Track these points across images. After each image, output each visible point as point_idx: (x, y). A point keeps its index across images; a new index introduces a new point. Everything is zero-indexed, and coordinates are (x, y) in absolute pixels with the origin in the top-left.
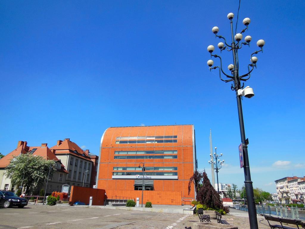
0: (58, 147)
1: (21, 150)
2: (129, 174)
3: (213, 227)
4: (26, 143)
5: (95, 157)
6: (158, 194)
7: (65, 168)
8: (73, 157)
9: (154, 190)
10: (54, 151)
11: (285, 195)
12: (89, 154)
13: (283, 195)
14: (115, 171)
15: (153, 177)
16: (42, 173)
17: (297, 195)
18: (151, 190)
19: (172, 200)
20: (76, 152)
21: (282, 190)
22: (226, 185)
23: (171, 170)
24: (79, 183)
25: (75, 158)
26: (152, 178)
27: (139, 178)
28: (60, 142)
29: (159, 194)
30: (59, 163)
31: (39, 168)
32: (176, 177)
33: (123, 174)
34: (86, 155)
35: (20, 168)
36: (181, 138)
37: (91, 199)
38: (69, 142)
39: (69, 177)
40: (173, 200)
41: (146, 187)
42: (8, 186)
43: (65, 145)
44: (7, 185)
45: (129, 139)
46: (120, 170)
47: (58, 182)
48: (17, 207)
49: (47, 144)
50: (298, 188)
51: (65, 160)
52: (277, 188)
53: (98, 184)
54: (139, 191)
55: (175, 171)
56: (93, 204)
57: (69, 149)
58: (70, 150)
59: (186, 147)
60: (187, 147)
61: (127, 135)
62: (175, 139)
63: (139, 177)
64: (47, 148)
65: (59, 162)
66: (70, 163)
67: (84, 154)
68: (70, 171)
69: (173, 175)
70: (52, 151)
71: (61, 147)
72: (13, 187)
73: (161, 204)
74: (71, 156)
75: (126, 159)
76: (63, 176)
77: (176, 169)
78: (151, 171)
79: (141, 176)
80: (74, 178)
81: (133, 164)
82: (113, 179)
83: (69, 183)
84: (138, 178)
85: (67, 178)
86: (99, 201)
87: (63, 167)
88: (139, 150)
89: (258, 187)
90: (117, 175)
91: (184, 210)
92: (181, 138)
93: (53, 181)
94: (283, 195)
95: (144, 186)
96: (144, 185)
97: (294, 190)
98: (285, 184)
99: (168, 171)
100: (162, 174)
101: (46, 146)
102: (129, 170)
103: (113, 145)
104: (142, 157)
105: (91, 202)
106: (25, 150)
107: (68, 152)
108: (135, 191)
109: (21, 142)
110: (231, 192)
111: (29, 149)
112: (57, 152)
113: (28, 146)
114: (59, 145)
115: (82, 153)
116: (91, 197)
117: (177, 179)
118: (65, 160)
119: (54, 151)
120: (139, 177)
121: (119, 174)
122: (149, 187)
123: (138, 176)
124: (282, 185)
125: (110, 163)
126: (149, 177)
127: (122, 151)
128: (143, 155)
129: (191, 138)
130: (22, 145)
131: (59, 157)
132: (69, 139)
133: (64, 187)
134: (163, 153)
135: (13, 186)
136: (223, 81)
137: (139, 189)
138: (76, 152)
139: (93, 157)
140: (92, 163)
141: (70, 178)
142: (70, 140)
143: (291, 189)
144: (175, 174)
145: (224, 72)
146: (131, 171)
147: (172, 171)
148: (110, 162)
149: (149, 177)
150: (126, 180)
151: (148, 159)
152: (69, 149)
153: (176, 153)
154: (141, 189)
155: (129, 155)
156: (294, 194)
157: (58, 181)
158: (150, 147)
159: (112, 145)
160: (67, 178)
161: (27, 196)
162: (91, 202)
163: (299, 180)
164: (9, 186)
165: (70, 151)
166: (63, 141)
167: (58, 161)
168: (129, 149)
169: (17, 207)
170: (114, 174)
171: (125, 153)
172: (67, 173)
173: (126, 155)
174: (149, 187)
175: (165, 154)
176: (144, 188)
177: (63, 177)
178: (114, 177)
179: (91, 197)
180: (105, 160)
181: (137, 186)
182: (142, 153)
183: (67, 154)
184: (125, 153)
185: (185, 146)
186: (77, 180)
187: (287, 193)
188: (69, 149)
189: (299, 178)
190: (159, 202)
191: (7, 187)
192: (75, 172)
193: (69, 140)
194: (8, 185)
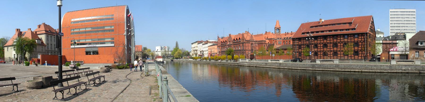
0: (38, 29)
6: (98, 57)
7: (44, 43)
8: (48, 35)
9: (99, 54)
10: (36, 32)
11: (195, 52)
13: (194, 52)
15: (97, 45)
17: (201, 52)
18: (97, 54)
19: (108, 60)
20: (50, 32)
21: (194, 49)
22: (164, 47)
23: (110, 40)
25: (50, 36)
26: (97, 46)
27: (88, 47)
28: (39, 26)
30: (39, 40)
32: (113, 45)
34: (57, 33)
36: (116, 16)
38: (45, 25)
39: (48, 48)
40: (108, 60)
43: (43, 28)
44: (15, 55)
45: (86, 19)
49: (31, 29)
50: (202, 48)
51: (43, 37)
52: (192, 48)
53: (416, 21)
54: (89, 55)
65: (40, 40)
66: (47, 39)
67: (56, 32)
68: (48, 44)
69: (111, 44)
70: (35, 33)
71: (40, 29)
74: (46, 34)
77: (113, 39)
79: (89, 45)
80: (51, 48)
82: (71, 48)
85: (46, 49)
87: (42, 42)
89: (183, 48)
92: (116, 16)
94: (194, 52)
97: (200, 49)
98: (196, 45)
99: (108, 41)
105: (46, 64)
107: (44, 32)
108: (86, 55)
110: (166, 51)
111: (22, 33)
113: (21, 31)
116: (46, 61)
117: (114, 46)
118: (43, 37)
122: (95, 52)
124: (194, 46)
126: (95, 45)
127: (76, 29)
129: (123, 16)
131: (40, 36)
132: (45, 23)
133: (39, 55)
135: (18, 55)
138: (50, 32)
142: (45, 24)
143: (199, 48)
144: (112, 42)
147: (110, 41)
148: (69, 37)
149: (95, 45)
150: (80, 48)
151: (94, 33)
153: (113, 28)
154: (90, 54)
156: (199, 51)
158: (95, 25)
160: (46, 49)
162: (46, 64)
163: (203, 43)
164: (16, 55)
165: (46, 31)
166: (41, 24)
167: (38, 39)
168: (80, 27)
171: (78, 30)
172: (46, 46)
174: (95, 52)
176: (92, 53)
177: (43, 48)
179: (46, 61)
181: (88, 52)
183: (44, 34)
185: (119, 22)
187: (196, 51)
189: (203, 42)
190: (99, 62)
193: (45, 24)
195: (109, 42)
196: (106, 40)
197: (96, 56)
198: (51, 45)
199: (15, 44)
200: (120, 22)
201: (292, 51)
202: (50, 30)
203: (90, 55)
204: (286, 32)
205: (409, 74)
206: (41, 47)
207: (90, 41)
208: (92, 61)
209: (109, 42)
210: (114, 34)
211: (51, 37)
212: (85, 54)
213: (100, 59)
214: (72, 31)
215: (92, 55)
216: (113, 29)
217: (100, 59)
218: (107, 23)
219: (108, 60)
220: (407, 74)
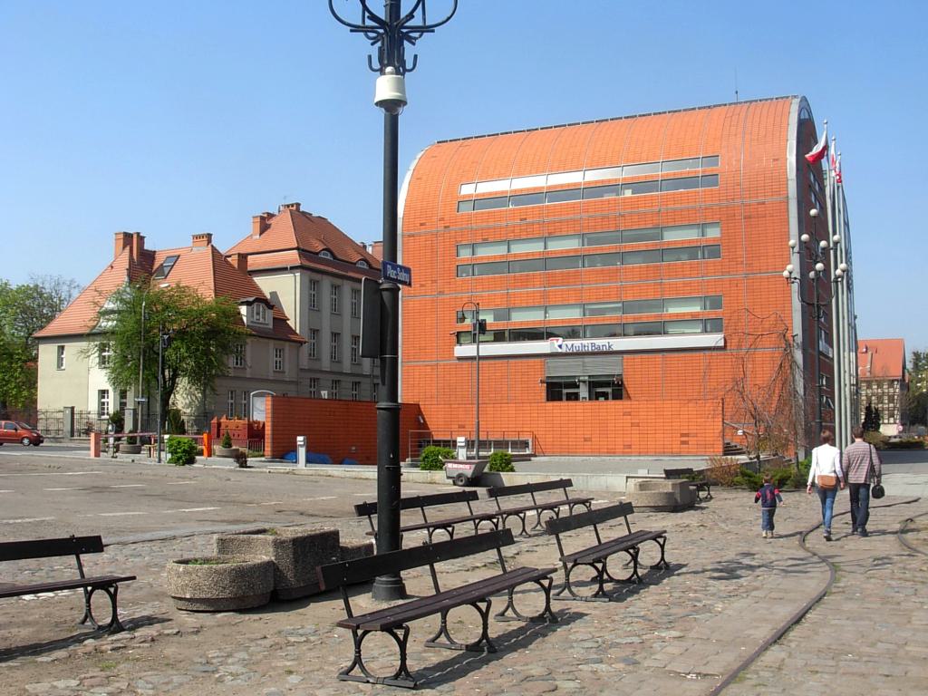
0: (258, 242)
1: (127, 267)
3: (258, 539)
7: (291, 323)
8: (317, 277)
10: (243, 258)
15: (619, 344)
19: (682, 435)
23: (696, 309)
24: (357, 380)
25: (326, 283)
26: (615, 348)
27: (564, 350)
28: (265, 223)
30: (262, 306)
32: (714, 339)
37: (301, 446)
38: (301, 218)
39: (314, 356)
43: (284, 233)
44: (103, 393)
47: (271, 378)
49: (209, 236)
51: (286, 291)
55: (712, 313)
56: (309, 461)
57: (296, 245)
58: (303, 250)
59: (759, 204)
60: (764, 203)
62: (710, 170)
63: (560, 346)
64: (214, 249)
65: (270, 304)
66: (311, 303)
68: (315, 332)
69: (705, 331)
70: (234, 261)
71: (271, 240)
73: (640, 454)
74: (309, 273)
76: (287, 355)
77: (716, 303)
78: (611, 319)
79: (569, 342)
80: (335, 358)
81: (534, 292)
82: (460, 359)
83: (359, 383)
84: (560, 350)
86: (354, 448)
87: (281, 321)
91: (627, 477)
93: (248, 376)
95: (584, 382)
96: (587, 378)
99: (684, 314)
100: (658, 329)
103: (447, 218)
105: (302, 452)
106: (140, 263)
107: (293, 257)
108: (550, 404)
109: (122, 236)
112: (252, 263)
113: (150, 249)
114: (261, 234)
115: (355, 258)
116: (300, 439)
117: (724, 348)
118: (286, 291)
119: (243, 258)
120: (560, 346)
122: (607, 384)
123: (556, 344)
125: (441, 297)
126: (602, 343)
127: (486, 242)
129: (780, 159)
130: (128, 248)
131: (266, 284)
132: (298, 205)
133: (256, 399)
135: (123, 394)
136: (449, 18)
137: (564, 397)
141: (338, 362)
144: (710, 325)
145: (343, 19)
146: (528, 323)
148: (441, 293)
149: (602, 343)
150: (511, 361)
152: (297, 249)
153: (713, 233)
155: (515, 255)
159: (442, 219)
160: (305, 363)
161: (196, 434)
162: (302, 452)
164: (111, 394)
165: (303, 252)
166: (276, 213)
167: (258, 300)
168: (513, 232)
172: (301, 343)
174: (607, 384)
175: (669, 243)
176: (583, 392)
179: (300, 439)
180: (422, 286)
181: (559, 385)
182: (572, 245)
183: (293, 268)
184: (500, 251)
185: (754, 201)
188: (297, 249)
190: (630, 446)
192: (336, 336)
193: (298, 209)
195: (692, 319)
196: (673, 310)
197: (610, 407)
199: (107, 324)
200: (761, 199)
203: (571, 403)
206: (272, 352)
207: (572, 315)
208: (585, 440)
209: (692, 319)
211: (335, 288)
212: (544, 394)
214: (465, 254)
215: (588, 403)
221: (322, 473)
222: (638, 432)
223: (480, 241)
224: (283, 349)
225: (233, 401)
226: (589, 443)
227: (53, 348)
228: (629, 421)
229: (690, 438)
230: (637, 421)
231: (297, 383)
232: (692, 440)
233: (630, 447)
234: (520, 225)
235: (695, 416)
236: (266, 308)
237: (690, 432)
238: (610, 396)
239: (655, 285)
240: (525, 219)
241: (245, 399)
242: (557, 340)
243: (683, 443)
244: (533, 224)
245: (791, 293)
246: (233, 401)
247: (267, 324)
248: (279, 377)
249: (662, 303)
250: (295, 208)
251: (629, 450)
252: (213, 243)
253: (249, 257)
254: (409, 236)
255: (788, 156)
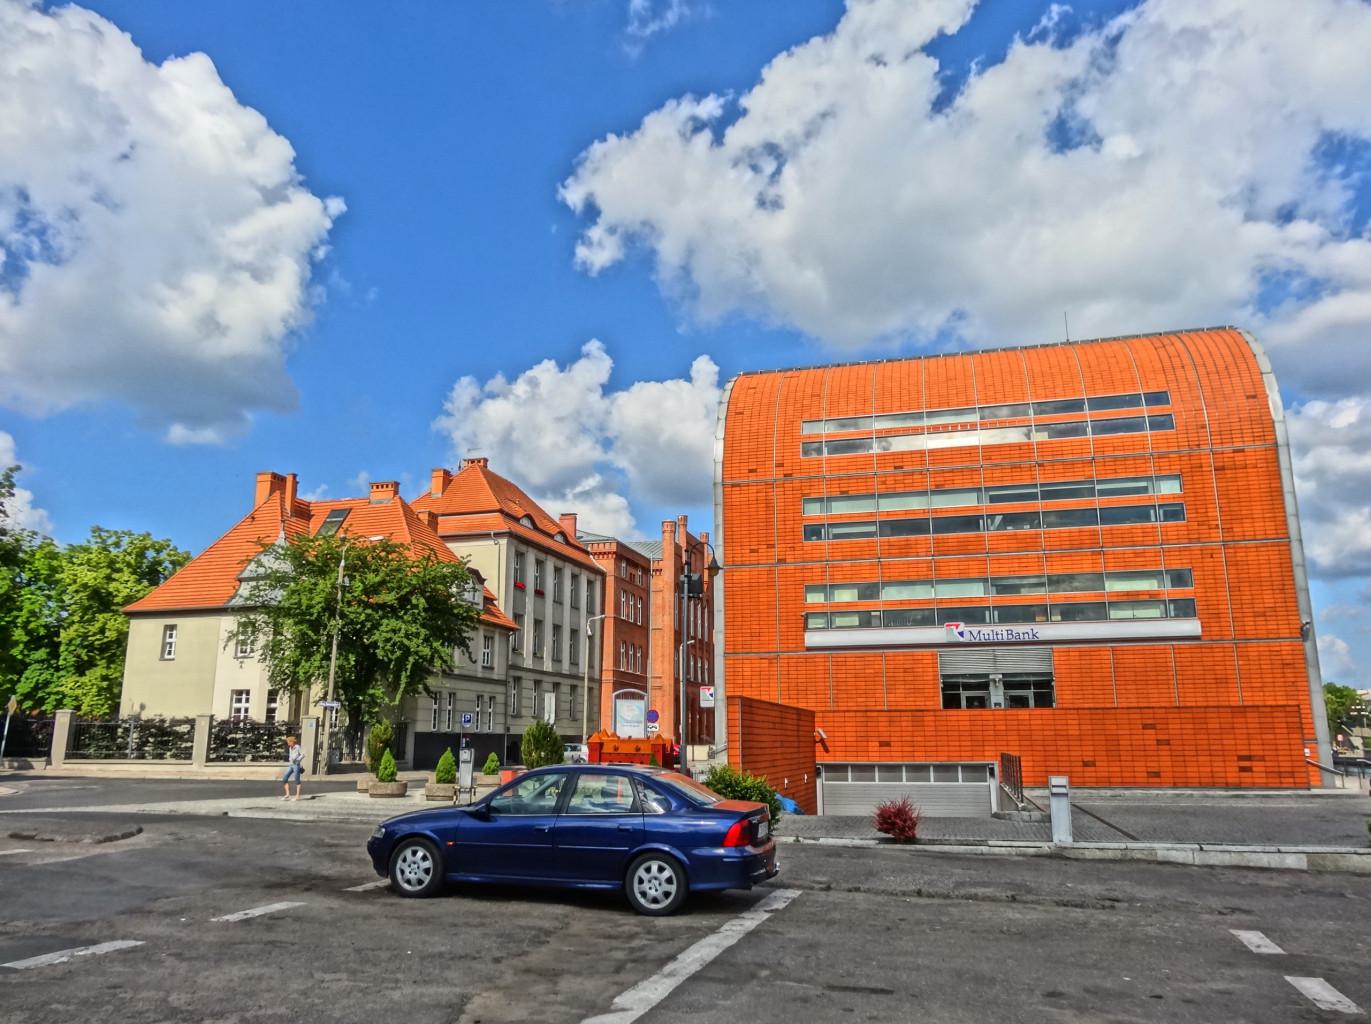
2: (897, 617)
4: (295, 483)
5: (614, 548)
8: (523, 548)
12: (578, 534)
14: (813, 606)
16: (423, 632)
19: (1241, 758)
24: (557, 679)
27: (966, 639)
29: (1153, 727)
31: (404, 601)
32: (1191, 627)
33: (866, 622)
35: (310, 607)
40: (1249, 758)
41: (1008, 686)
42: (247, 701)
44: (240, 694)
46: (846, 596)
47: (480, 675)
48: (725, 860)
49: (397, 484)
55: (1182, 592)
59: (1235, 452)
61: (860, 407)
69: (1166, 616)
70: (424, 517)
72: (273, 705)
74: (515, 542)
75: (875, 539)
77: (1179, 579)
79: (975, 629)
81: (918, 562)
82: (809, 649)
84: (961, 639)
87: (489, 600)
88: (947, 487)
90: (830, 626)
93: (495, 677)
100: (1098, 611)
101: (396, 492)
102: (891, 595)
103: (787, 463)
104: (970, 522)
108: (951, 712)
115: (553, 530)
119: (433, 517)
120: (961, 634)
121: (839, 621)
122: (1025, 685)
123: (956, 632)
125: (782, 567)
126: (1022, 630)
127: (845, 496)
128: (976, 509)
132: (486, 460)
134: (1145, 489)
135: (272, 696)
137: (964, 703)
139: (601, 548)
140: (599, 578)
144: (1184, 609)
148: (781, 561)
157: (480, 669)
168: (884, 483)
169: (725, 860)
170: (813, 623)
173: (871, 514)
174: (1025, 685)
176: (997, 695)
178: (812, 639)
180: (752, 551)
181: (956, 686)
186: (566, 667)
188: (501, 511)
190: (1157, 775)
191: (243, 705)
194: (248, 692)
195: (1151, 599)
197: (249, 711)
198: (557, 628)
199: (278, 595)
200: (1238, 445)
201: (240, 592)
202: (528, 516)
204: (143, 707)
205: (1327, 876)
207: (976, 591)
208: (1085, 764)
209: (1151, 599)
210: (1190, 540)
213: (1168, 743)
214: (813, 511)
216: (1174, 497)
217: (1168, 743)
218: (1117, 453)
219: (1249, 758)
220: (963, 901)
221: (1138, 855)
222: (1169, 753)
223: (838, 494)
224: (493, 638)
225: (450, 708)
226: (1093, 769)
227: (156, 625)
228: (1154, 737)
229: (1254, 764)
230: (1166, 737)
231: (504, 683)
232: (1258, 766)
233: (1157, 775)
234: (894, 475)
235: (1258, 731)
236: (476, 581)
237: (1253, 753)
238: (1032, 702)
239: (1093, 553)
240: (901, 467)
241: (435, 704)
242: (957, 626)
243: (1243, 769)
244: (912, 474)
245: (725, 610)
246: (450, 708)
247: (477, 604)
248: (487, 675)
249: (1099, 578)
250: (482, 464)
251: (1157, 780)
252: (401, 494)
253: (440, 518)
254: (733, 486)
255: (1268, 392)
